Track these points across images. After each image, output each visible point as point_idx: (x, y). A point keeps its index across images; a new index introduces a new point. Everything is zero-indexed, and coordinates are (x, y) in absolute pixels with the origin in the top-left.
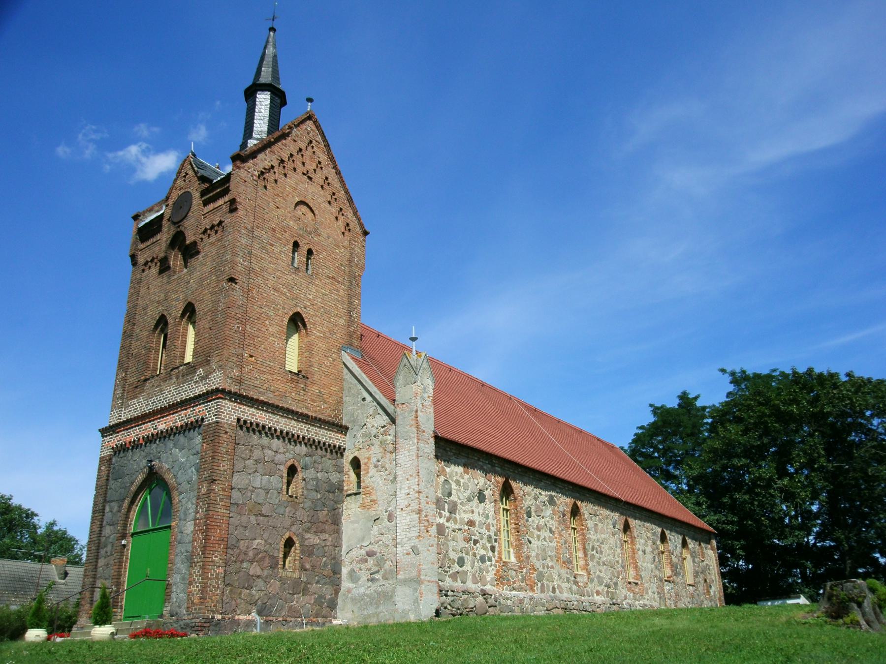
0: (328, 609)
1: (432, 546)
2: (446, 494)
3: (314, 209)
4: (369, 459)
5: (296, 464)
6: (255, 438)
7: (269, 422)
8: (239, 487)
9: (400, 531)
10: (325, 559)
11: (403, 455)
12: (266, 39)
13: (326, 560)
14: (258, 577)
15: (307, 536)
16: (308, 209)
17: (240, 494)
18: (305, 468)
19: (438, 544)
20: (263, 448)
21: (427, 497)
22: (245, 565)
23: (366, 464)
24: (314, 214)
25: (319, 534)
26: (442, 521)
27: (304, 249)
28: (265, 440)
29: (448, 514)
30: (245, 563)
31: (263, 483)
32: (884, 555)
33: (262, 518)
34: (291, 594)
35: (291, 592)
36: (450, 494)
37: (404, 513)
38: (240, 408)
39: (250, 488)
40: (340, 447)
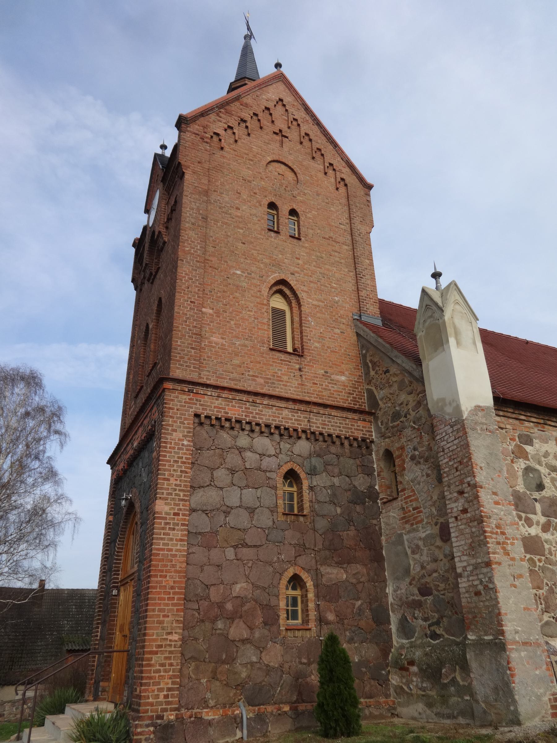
0: (372, 682)
1: (520, 576)
2: (534, 486)
3: (294, 167)
4: (402, 448)
5: (297, 469)
6: (225, 437)
7: (246, 416)
8: (205, 508)
9: (459, 554)
10: (359, 603)
11: (444, 434)
12: (242, 42)
13: (362, 604)
14: (244, 641)
15: (324, 569)
16: (280, 164)
17: (207, 518)
18: (312, 472)
19: (531, 571)
20: (241, 450)
21: (495, 494)
22: (220, 625)
23: (400, 456)
24: (295, 174)
25: (345, 566)
26: (534, 531)
27: (284, 210)
28: (243, 440)
29: (543, 520)
30: (219, 622)
31: (243, 499)
32: (556, 518)
33: (245, 550)
34: (304, 664)
35: (304, 661)
36: (540, 487)
37: (460, 523)
38: (293, 423)
39: (224, 508)
40: (364, 440)
